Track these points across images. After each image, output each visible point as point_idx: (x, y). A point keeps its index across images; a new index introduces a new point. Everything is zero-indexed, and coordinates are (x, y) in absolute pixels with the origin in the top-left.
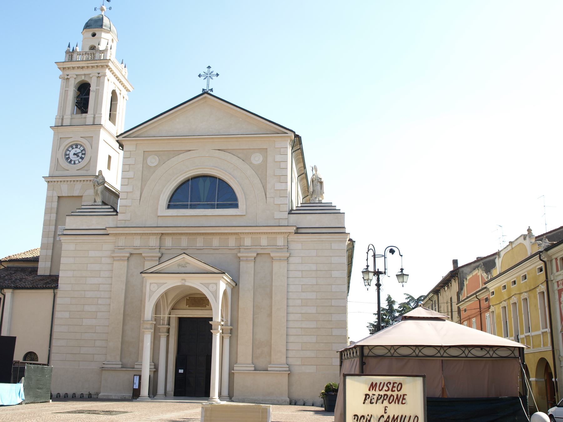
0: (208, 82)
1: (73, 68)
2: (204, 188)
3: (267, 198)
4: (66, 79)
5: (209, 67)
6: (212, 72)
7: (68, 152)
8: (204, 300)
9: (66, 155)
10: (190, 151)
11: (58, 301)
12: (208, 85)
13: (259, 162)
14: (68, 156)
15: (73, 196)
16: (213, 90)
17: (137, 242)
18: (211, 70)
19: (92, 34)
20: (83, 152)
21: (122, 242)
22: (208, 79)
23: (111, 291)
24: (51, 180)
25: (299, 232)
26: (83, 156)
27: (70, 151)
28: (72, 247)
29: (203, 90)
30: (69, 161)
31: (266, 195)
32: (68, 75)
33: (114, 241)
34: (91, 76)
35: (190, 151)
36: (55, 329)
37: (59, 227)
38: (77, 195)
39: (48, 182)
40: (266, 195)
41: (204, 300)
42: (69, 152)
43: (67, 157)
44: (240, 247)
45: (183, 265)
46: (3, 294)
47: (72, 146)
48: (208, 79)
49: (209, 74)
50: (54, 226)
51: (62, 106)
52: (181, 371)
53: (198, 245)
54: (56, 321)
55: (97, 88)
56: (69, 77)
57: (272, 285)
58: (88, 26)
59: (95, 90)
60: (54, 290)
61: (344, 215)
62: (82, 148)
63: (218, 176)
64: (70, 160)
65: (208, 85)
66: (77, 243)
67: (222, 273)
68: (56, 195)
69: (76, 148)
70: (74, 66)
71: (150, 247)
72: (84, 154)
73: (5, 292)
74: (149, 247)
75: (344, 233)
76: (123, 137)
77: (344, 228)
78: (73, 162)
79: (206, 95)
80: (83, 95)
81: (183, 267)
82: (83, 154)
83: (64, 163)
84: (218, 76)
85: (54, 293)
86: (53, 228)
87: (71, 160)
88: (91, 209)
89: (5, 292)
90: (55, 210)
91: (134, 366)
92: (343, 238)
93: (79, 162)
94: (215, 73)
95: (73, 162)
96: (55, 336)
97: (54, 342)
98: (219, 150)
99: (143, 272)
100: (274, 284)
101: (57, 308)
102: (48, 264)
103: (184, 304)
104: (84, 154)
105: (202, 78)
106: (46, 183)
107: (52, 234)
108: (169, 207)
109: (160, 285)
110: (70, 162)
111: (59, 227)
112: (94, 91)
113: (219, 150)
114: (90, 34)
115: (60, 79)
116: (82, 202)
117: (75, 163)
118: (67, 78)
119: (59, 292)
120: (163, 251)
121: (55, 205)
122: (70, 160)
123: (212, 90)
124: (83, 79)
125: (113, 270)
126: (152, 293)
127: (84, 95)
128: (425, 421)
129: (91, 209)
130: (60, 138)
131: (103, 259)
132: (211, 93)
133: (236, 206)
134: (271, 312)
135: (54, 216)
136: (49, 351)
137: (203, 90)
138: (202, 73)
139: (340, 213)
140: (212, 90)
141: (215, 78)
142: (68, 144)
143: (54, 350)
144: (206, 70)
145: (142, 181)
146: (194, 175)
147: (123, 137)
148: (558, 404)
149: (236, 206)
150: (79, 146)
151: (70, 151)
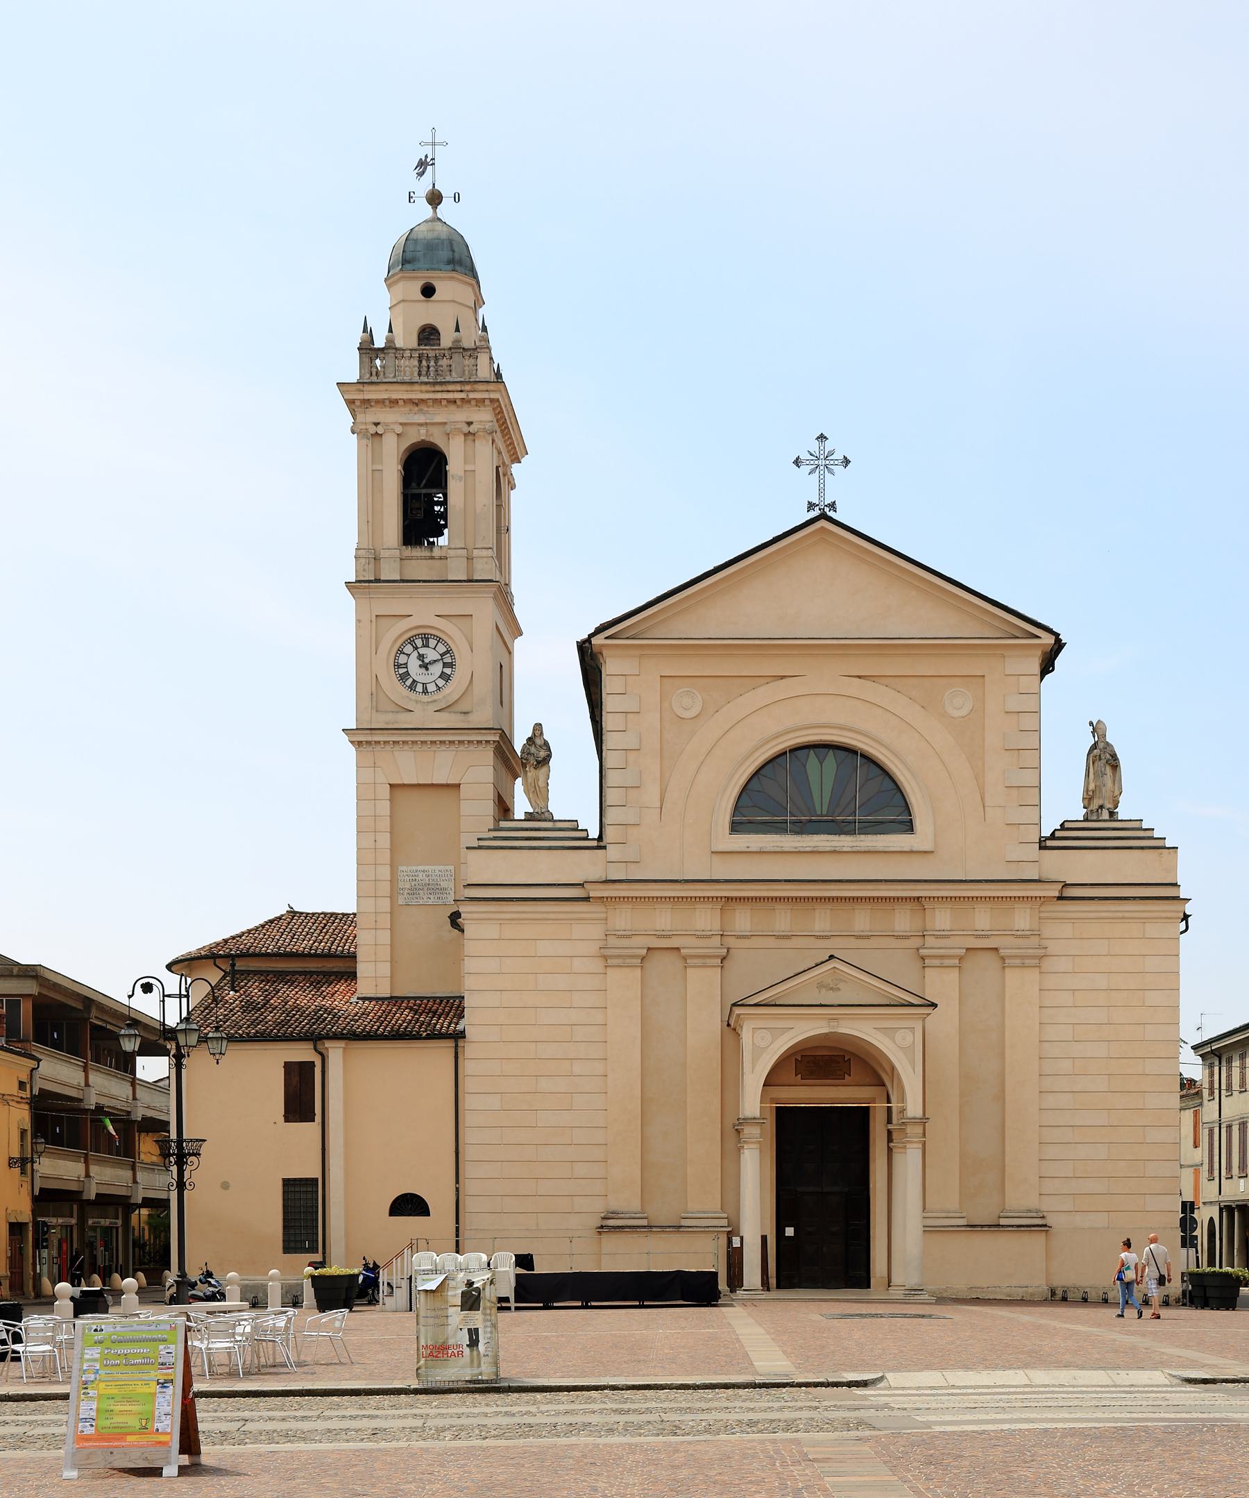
0: (822, 481)
1: (394, 402)
2: (822, 774)
3: (986, 808)
4: (370, 436)
5: (822, 438)
6: (832, 453)
7: (403, 659)
8: (838, 1062)
9: (398, 666)
10: (783, 677)
11: (468, 1067)
12: (822, 491)
13: (964, 712)
14: (405, 670)
15: (432, 785)
16: (838, 505)
17: (664, 919)
18: (829, 446)
19: (424, 284)
20: (448, 659)
21: (622, 919)
22: (822, 472)
23: (606, 1042)
24: (369, 739)
25: (1065, 895)
26: (448, 671)
27: (408, 655)
28: (491, 931)
29: (811, 506)
30: (409, 682)
31: (982, 799)
32: (377, 424)
33: (603, 916)
34: (448, 428)
35: (783, 677)
36: (468, 1137)
37: (401, 868)
38: (444, 782)
39: (358, 744)
40: (982, 799)
41: (838, 1062)
42: (406, 657)
43: (402, 671)
44: (925, 933)
45: (831, 986)
46: (321, 1054)
47: (414, 640)
48: (822, 472)
49: (822, 457)
50: (388, 868)
51: (370, 520)
52: (790, 1232)
53: (817, 927)
54: (468, 1119)
55: (469, 468)
56: (380, 430)
57: (1002, 1026)
58: (409, 262)
59: (462, 474)
60: (456, 1041)
61: (1176, 852)
62: (441, 648)
63: (860, 749)
64: (410, 680)
65: (822, 491)
66: (504, 922)
67: (929, 1006)
68: (384, 778)
69: (424, 646)
70: (394, 396)
71: (697, 933)
72: (451, 665)
73: (327, 1049)
74: (696, 931)
75: (1177, 898)
76: (606, 638)
77: (1175, 885)
78: (419, 688)
79: (823, 523)
80: (422, 485)
81: (831, 989)
82: (445, 665)
83: (397, 691)
84: (846, 465)
85: (456, 1046)
86: (385, 872)
87: (414, 681)
88: (527, 829)
89: (327, 1049)
90: (385, 824)
91: (680, 1222)
92: (1174, 911)
93: (439, 688)
94: (838, 456)
95: (419, 688)
96: (468, 1153)
97: (468, 1170)
98: (859, 677)
99: (739, 1003)
100: (1007, 1022)
101: (467, 1085)
102: (385, 969)
103: (792, 1077)
104: (451, 665)
105: (805, 469)
106: (352, 750)
107: (385, 888)
108: (736, 827)
109: (776, 1033)
110: (412, 687)
111: (401, 868)
112: (461, 477)
113: (859, 677)
114: (416, 287)
115: (353, 433)
116: (460, 800)
117: (425, 691)
118: (373, 432)
119: (470, 1050)
120: (731, 942)
121: (384, 808)
122: (410, 681)
123: (832, 506)
124: (423, 438)
125: (606, 990)
126: (758, 1052)
127: (426, 487)
128: (2, 1395)
129: (527, 829)
130: (376, 616)
131: (576, 961)
132: (831, 514)
133: (908, 827)
134: (1003, 1091)
135: (384, 840)
136: (457, 1189)
137: (811, 506)
138: (805, 456)
139: (1165, 848)
140: (832, 506)
141: (838, 469)
142: (401, 635)
143: (469, 1187)
144: (814, 446)
145: (661, 758)
146: (797, 744)
147: (606, 638)
148: (477, 1294)
149: (908, 827)
150: (432, 643)
151: (408, 655)
